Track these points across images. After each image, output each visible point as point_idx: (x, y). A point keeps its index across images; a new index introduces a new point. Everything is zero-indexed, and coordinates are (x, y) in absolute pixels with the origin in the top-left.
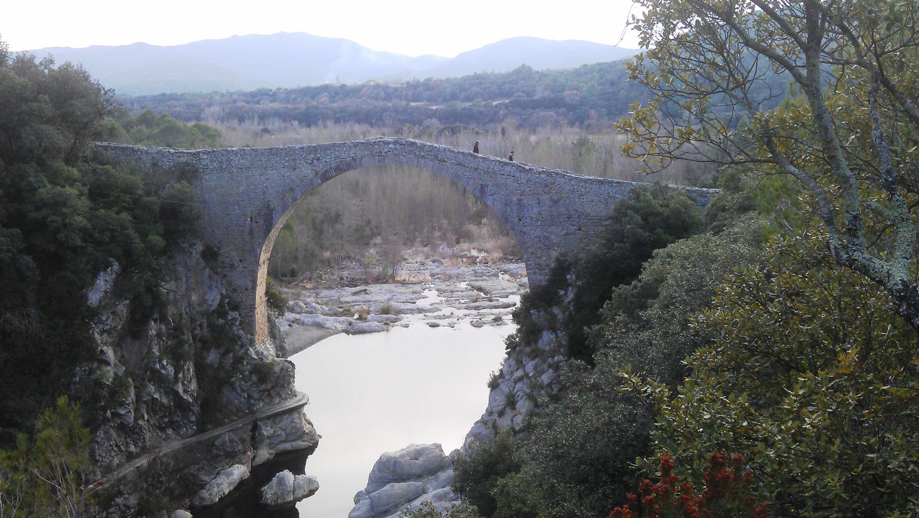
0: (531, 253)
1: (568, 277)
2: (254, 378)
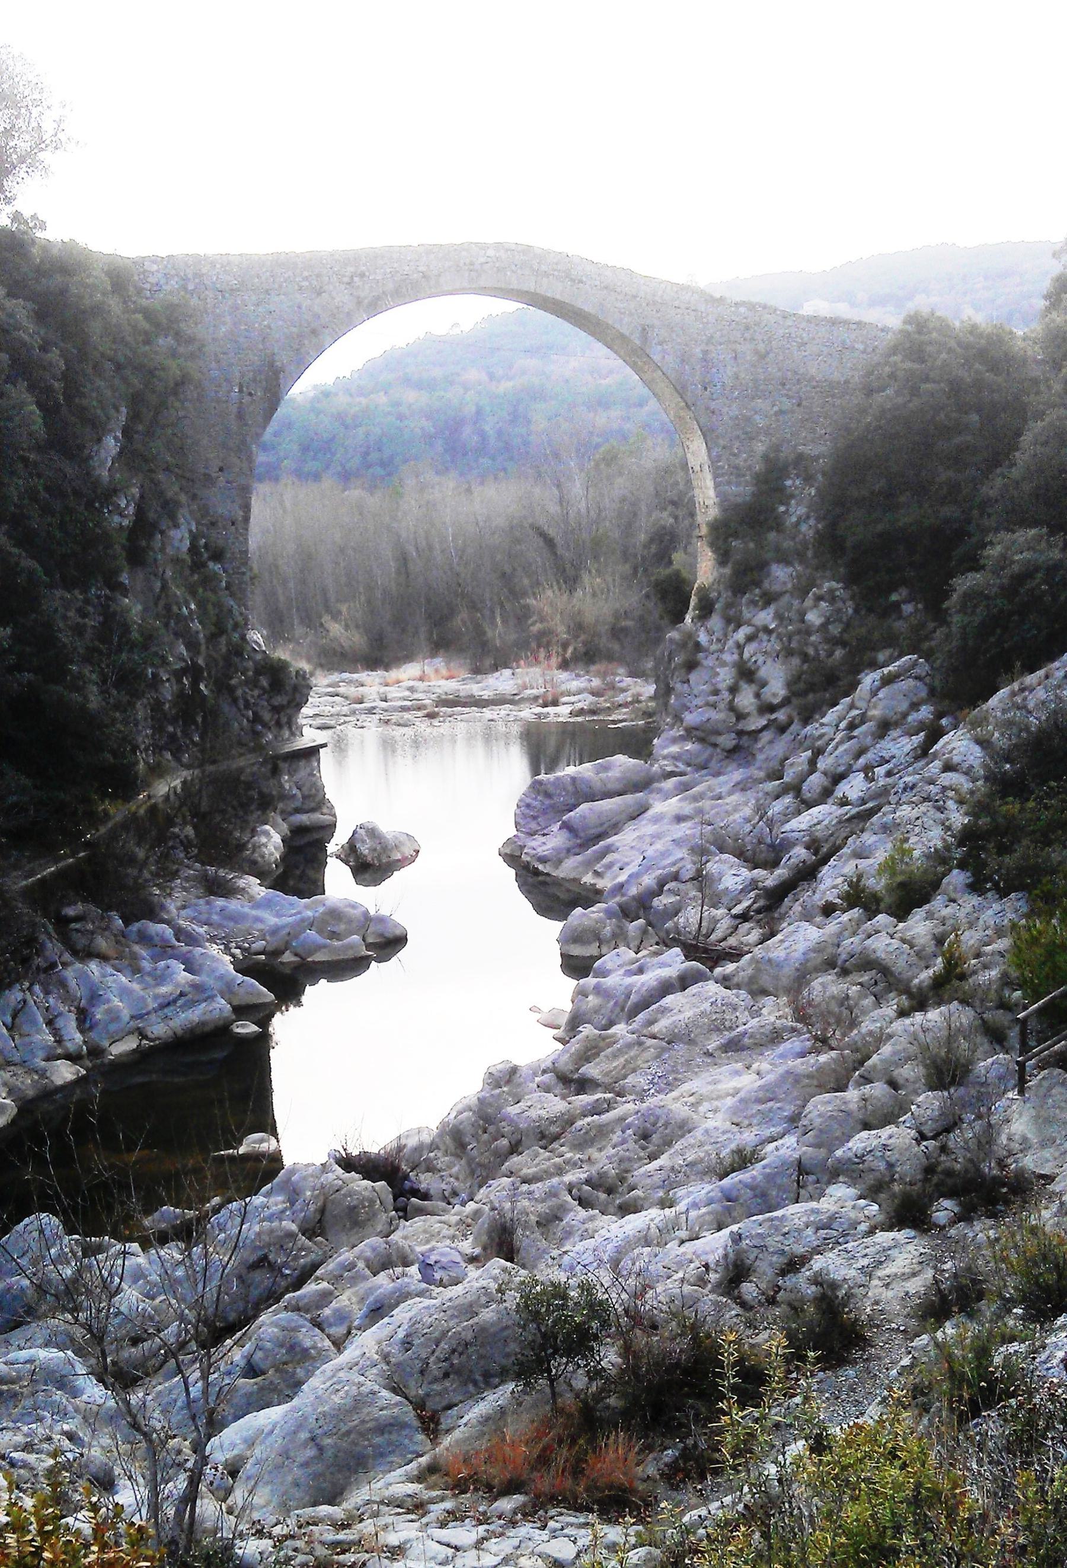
0: (724, 448)
1: (789, 483)
2: (264, 682)
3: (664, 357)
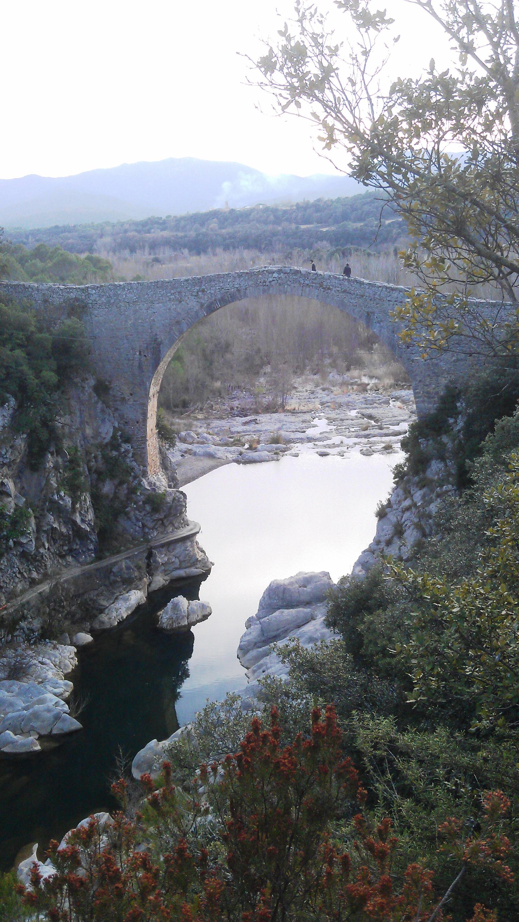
1: (458, 404)
2: (148, 508)
3: (381, 330)
